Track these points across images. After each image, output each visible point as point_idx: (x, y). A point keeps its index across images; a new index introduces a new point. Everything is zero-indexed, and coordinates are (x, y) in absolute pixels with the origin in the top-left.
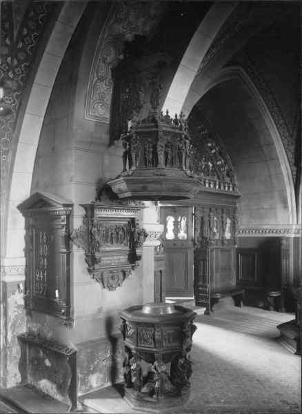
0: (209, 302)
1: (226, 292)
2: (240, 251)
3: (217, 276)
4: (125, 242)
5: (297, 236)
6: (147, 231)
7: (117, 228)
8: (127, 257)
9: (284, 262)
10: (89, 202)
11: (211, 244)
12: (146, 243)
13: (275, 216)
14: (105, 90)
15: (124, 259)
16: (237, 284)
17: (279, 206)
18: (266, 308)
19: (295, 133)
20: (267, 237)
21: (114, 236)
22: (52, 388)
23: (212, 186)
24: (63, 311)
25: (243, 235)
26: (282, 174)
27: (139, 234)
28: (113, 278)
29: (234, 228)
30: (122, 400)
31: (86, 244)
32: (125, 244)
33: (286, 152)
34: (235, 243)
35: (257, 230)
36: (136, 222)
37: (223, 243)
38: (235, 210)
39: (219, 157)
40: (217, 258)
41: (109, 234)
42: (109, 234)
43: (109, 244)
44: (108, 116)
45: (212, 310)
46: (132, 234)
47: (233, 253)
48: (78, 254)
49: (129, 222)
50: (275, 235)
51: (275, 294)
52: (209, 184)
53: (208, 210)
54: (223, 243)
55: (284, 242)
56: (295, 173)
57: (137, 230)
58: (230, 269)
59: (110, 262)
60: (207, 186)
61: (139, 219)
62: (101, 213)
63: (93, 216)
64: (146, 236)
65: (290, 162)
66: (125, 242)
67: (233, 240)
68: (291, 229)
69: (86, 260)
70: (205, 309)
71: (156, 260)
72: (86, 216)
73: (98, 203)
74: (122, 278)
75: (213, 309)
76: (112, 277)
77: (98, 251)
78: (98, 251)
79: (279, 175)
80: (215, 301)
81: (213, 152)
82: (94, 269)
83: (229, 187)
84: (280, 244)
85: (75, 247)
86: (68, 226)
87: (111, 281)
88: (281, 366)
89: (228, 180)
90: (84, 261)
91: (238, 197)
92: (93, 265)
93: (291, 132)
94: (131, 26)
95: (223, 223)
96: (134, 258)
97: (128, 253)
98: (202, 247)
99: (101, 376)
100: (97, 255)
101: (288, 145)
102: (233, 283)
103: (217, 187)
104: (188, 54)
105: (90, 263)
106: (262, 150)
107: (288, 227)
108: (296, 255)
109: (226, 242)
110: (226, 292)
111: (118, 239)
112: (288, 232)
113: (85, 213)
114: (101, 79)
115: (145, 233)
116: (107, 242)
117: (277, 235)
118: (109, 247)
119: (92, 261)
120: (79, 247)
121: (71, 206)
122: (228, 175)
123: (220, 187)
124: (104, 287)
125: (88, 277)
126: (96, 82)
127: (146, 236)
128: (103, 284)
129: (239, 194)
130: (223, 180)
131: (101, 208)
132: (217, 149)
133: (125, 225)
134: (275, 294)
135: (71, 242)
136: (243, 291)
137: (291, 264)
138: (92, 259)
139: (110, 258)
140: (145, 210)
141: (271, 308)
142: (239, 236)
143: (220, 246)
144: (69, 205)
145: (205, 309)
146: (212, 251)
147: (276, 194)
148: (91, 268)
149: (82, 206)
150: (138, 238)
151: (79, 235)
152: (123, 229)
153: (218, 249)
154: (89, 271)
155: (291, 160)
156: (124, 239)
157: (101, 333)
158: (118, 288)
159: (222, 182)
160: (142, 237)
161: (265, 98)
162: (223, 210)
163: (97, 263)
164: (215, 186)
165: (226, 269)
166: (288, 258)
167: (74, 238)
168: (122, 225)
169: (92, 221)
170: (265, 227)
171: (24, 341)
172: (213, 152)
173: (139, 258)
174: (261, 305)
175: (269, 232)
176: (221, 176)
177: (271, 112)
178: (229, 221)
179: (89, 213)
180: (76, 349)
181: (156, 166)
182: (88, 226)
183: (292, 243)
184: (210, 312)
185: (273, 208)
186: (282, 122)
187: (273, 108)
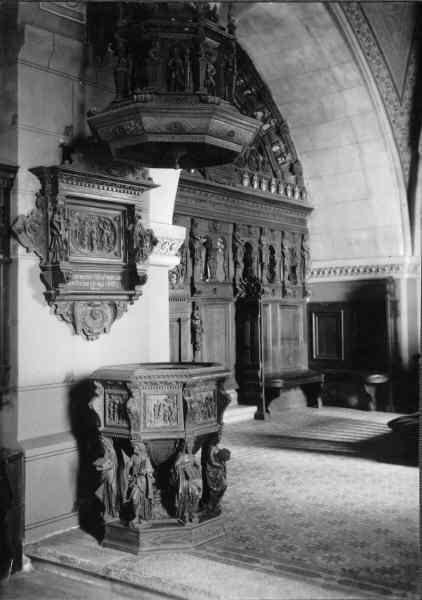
0: (263, 395)
1: (292, 380)
2: (313, 308)
4: (116, 249)
5: (414, 276)
6: (156, 235)
7: (103, 222)
8: (119, 278)
11: (263, 292)
12: (153, 258)
15: (113, 281)
16: (310, 366)
18: (363, 406)
21: (94, 236)
28: (93, 316)
31: (42, 246)
32: (116, 254)
33: (392, 128)
34: (305, 294)
39: (276, 138)
40: (274, 316)
41: (87, 233)
42: (87, 233)
43: (86, 251)
45: (267, 411)
46: (129, 236)
47: (302, 312)
50: (372, 276)
51: (377, 379)
52: (260, 183)
53: (258, 230)
57: (138, 229)
58: (297, 339)
59: (87, 284)
60: (256, 186)
62: (66, 188)
63: (55, 191)
64: (154, 242)
66: (116, 249)
68: (402, 265)
69: (42, 276)
70: (254, 409)
71: (172, 299)
72: (42, 192)
73: (67, 165)
74: (110, 317)
75: (269, 409)
76: (91, 314)
77: (67, 260)
78: (67, 260)
80: (273, 393)
82: (58, 293)
84: (384, 286)
87: (90, 322)
88: (390, 490)
89: (291, 179)
90: (39, 279)
91: (310, 210)
92: (56, 285)
93: (400, 93)
96: (133, 280)
97: (121, 270)
100: (64, 266)
101: (395, 116)
102: (304, 366)
103: (273, 190)
105: (50, 281)
108: (412, 311)
111: (102, 242)
112: (398, 269)
115: (151, 236)
116: (84, 247)
118: (87, 255)
119: (53, 279)
120: (28, 251)
123: (278, 190)
124: (76, 333)
125: (47, 309)
127: (154, 242)
128: (75, 327)
130: (283, 178)
132: (273, 124)
134: (377, 379)
135: (12, 242)
136: (323, 376)
137: (406, 327)
138: (54, 275)
139: (89, 277)
140: (152, 192)
142: (315, 280)
143: (278, 296)
145: (254, 409)
146: (266, 305)
148: (52, 292)
149: (31, 170)
150: (141, 242)
151: (28, 226)
152: (112, 225)
153: (276, 301)
154: (49, 298)
155: (399, 142)
156: (114, 243)
158: (102, 336)
161: (345, 8)
162: (283, 233)
163: (63, 282)
165: (290, 339)
166: (396, 314)
168: (111, 218)
171: (45, 294)
173: (142, 280)
174: (354, 401)
175: (365, 271)
176: (279, 173)
177: (375, 78)
179: (49, 186)
184: (266, 415)
187: (359, 25)
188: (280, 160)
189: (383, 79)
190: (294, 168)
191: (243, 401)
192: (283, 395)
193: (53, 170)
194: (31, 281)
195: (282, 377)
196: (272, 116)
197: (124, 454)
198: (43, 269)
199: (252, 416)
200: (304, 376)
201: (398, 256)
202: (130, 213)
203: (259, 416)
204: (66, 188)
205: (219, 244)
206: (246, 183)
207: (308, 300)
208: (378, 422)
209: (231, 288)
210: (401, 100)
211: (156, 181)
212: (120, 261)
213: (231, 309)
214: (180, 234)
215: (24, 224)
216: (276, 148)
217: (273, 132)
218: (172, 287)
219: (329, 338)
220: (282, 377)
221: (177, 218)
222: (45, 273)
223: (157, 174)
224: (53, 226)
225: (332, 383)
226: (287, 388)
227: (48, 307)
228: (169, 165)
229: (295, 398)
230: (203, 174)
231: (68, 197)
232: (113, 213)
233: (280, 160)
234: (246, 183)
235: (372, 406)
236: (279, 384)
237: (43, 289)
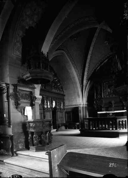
1: (63, 125)
2: (66, 112)
3: (59, 120)
9: (80, 114)
10: (16, 83)
13: (76, 101)
14: (19, 45)
16: (66, 122)
17: (77, 97)
18: (75, 129)
19: (81, 74)
20: (74, 107)
22: (4, 151)
23: (56, 91)
24: (7, 122)
25: (67, 107)
26: (78, 87)
27: (34, 98)
29: (64, 105)
30: (29, 151)
34: (64, 110)
35: (71, 105)
36: (33, 93)
37: (61, 110)
38: (64, 99)
43: (23, 100)
44: (21, 56)
46: (31, 97)
47: (64, 113)
48: (12, 102)
49: (30, 93)
51: (78, 124)
54: (61, 110)
55: (79, 108)
56: (81, 87)
57: (33, 96)
61: (34, 92)
62: (19, 88)
65: (80, 83)
67: (64, 109)
70: (56, 130)
71: (40, 109)
79: (77, 87)
80: (59, 127)
81: (56, 81)
83: (62, 92)
85: (10, 99)
86: (8, 92)
89: (61, 90)
91: (65, 95)
94: (29, 21)
95: (61, 104)
98: (55, 110)
99: (22, 144)
102: (65, 122)
104: (48, 36)
106: (73, 85)
107: (80, 103)
109: (62, 109)
110: (63, 125)
113: (14, 88)
114: (18, 42)
117: (77, 106)
121: (9, 84)
122: (61, 89)
123: (59, 92)
126: (16, 42)
127: (36, 98)
129: (65, 94)
131: (21, 86)
133: (29, 94)
140: (35, 89)
141: (77, 128)
143: (60, 110)
144: (7, 84)
147: (76, 94)
149: (12, 85)
154: (17, 108)
157: (21, 130)
159: (60, 90)
160: (35, 99)
164: (57, 91)
166: (80, 113)
167: (10, 96)
169: (17, 90)
170: (73, 104)
172: (56, 81)
178: (62, 103)
179: (15, 88)
180: (13, 135)
181: (40, 68)
182: (15, 92)
183: (81, 108)
185: (75, 98)
186: (75, 66)
188: (59, 86)
189: (71, 60)
190: (62, 88)
191: (54, 128)
192: (61, 127)
193: (16, 84)
194: (13, 105)
195: (61, 124)
196: (60, 99)
197: (46, 56)
198: (15, 102)
199: (55, 131)
200: (65, 124)
201: (80, 103)
202: (31, 93)
203: (57, 131)
204: (19, 88)
205: (47, 128)
206: (53, 90)
207: (65, 111)
208: (77, 131)
209: (51, 109)
210: (80, 75)
211: (36, 87)
212: (30, 102)
213: (51, 113)
214: (41, 97)
215: (11, 94)
216: (58, 84)
217: (58, 81)
218: (40, 107)
219: (69, 117)
220: (61, 124)
221: (40, 95)
222: (16, 104)
223: (36, 86)
224: (16, 95)
225: (70, 126)
226: (62, 126)
227: (16, 110)
228: (37, 83)
229: (63, 128)
230: (45, 88)
231: (19, 90)
232: (28, 93)
233: (59, 86)
234: (53, 90)
235: (77, 128)
236: (60, 125)
237: (15, 106)
